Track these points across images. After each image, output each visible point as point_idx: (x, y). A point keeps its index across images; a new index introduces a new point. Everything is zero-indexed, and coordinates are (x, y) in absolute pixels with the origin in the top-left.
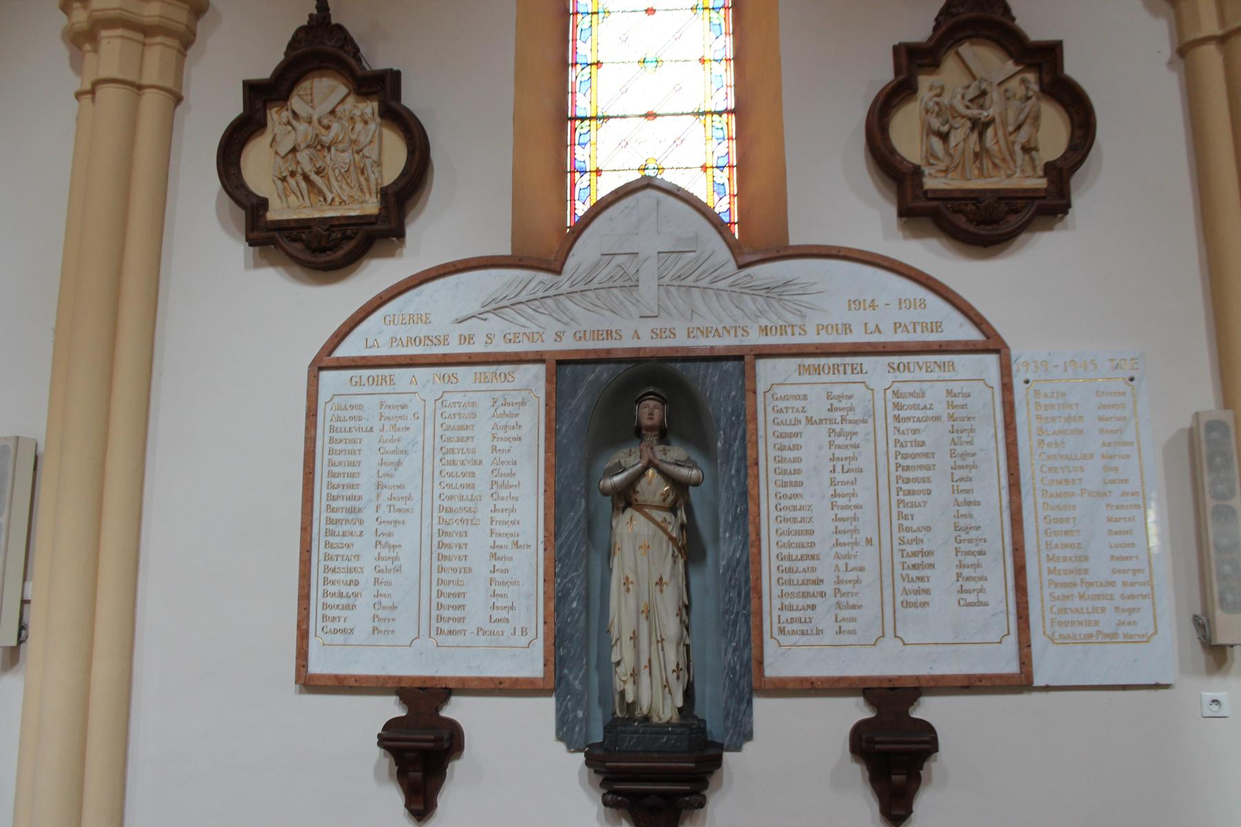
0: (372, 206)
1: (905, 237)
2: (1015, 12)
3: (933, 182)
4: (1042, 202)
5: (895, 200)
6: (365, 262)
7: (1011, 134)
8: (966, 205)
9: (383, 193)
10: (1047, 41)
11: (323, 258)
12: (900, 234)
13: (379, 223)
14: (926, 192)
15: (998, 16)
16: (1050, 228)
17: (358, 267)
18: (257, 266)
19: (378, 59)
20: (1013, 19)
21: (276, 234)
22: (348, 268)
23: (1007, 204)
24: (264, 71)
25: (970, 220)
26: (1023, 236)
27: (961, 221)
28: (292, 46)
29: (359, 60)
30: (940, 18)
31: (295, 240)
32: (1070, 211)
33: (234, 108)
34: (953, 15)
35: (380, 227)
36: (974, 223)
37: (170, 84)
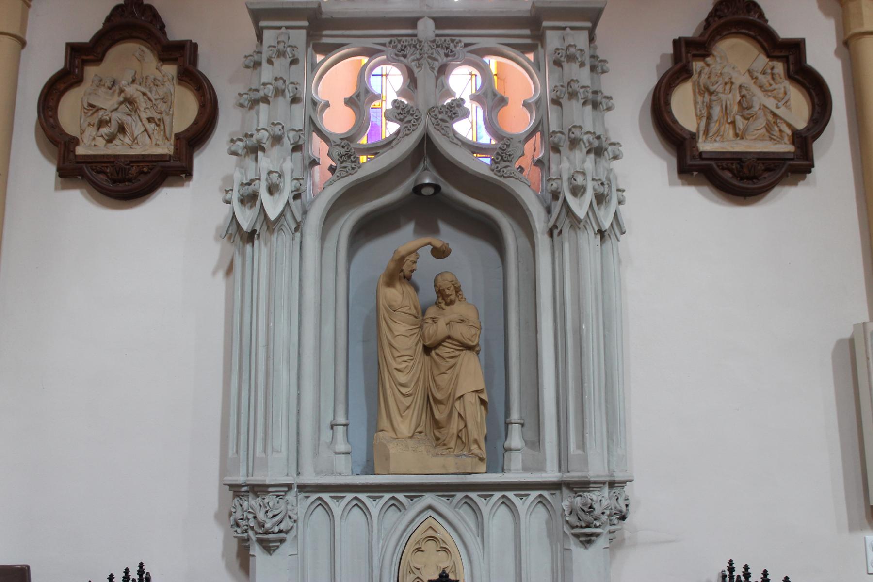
0: (166, 148)
1: (683, 184)
2: (767, 16)
3: (705, 146)
4: (791, 162)
5: (676, 155)
6: (160, 189)
7: (257, 179)
8: (732, 164)
9: (177, 138)
10: (791, 39)
11: (121, 187)
12: (680, 181)
13: (172, 161)
14: (701, 153)
15: (754, 17)
16: (795, 183)
17: (149, 197)
18: (64, 187)
19: (176, 32)
20: (767, 21)
21: (84, 166)
22: (142, 198)
23: (763, 164)
24: (85, 35)
25: (734, 175)
26: (776, 189)
27: (727, 175)
28: (108, 19)
29: (165, 33)
30: (710, 19)
31: (98, 172)
32: (813, 169)
33: (56, 62)
34: (720, 17)
35: (172, 163)
36: (739, 179)
37: (15, 31)
